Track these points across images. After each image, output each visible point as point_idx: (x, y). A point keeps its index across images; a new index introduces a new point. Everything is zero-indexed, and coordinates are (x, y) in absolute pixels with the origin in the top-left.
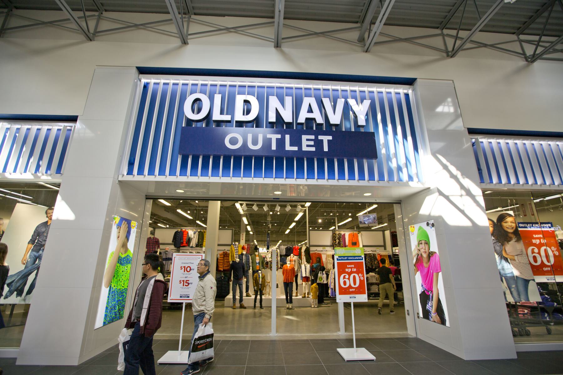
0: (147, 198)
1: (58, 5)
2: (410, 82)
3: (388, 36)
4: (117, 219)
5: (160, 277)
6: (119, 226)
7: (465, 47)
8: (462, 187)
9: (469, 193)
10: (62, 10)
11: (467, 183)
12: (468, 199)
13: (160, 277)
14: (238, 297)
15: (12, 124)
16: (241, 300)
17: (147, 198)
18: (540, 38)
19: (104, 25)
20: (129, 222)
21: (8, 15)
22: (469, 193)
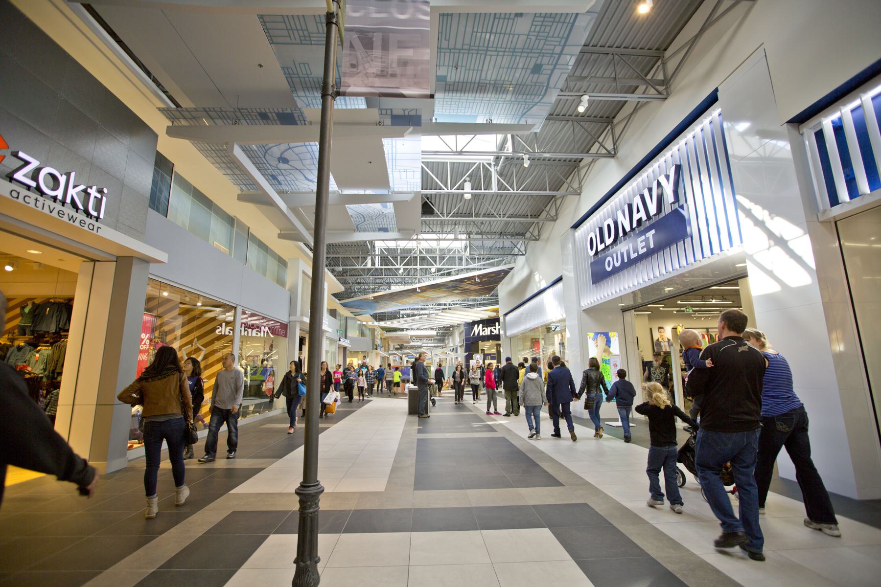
0: (623, 312)
1: (621, 101)
2: (712, 99)
3: (623, 120)
4: (591, 335)
5: (251, 408)
6: (595, 339)
7: (617, 137)
8: (771, 235)
9: (781, 242)
10: (627, 101)
11: (781, 226)
12: (778, 250)
13: (251, 408)
14: (380, 388)
15: (842, 107)
16: (381, 390)
17: (623, 312)
18: (599, 142)
19: (671, 65)
20: (606, 335)
21: (664, 64)
22: (781, 242)
